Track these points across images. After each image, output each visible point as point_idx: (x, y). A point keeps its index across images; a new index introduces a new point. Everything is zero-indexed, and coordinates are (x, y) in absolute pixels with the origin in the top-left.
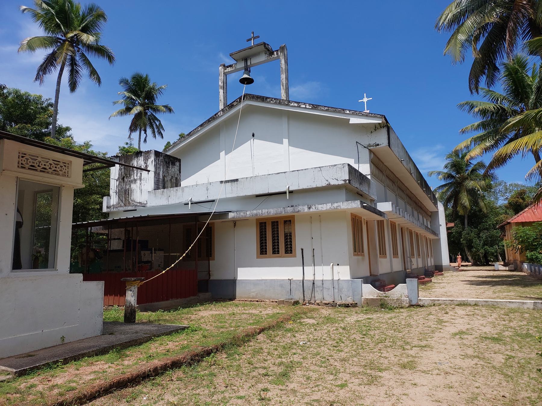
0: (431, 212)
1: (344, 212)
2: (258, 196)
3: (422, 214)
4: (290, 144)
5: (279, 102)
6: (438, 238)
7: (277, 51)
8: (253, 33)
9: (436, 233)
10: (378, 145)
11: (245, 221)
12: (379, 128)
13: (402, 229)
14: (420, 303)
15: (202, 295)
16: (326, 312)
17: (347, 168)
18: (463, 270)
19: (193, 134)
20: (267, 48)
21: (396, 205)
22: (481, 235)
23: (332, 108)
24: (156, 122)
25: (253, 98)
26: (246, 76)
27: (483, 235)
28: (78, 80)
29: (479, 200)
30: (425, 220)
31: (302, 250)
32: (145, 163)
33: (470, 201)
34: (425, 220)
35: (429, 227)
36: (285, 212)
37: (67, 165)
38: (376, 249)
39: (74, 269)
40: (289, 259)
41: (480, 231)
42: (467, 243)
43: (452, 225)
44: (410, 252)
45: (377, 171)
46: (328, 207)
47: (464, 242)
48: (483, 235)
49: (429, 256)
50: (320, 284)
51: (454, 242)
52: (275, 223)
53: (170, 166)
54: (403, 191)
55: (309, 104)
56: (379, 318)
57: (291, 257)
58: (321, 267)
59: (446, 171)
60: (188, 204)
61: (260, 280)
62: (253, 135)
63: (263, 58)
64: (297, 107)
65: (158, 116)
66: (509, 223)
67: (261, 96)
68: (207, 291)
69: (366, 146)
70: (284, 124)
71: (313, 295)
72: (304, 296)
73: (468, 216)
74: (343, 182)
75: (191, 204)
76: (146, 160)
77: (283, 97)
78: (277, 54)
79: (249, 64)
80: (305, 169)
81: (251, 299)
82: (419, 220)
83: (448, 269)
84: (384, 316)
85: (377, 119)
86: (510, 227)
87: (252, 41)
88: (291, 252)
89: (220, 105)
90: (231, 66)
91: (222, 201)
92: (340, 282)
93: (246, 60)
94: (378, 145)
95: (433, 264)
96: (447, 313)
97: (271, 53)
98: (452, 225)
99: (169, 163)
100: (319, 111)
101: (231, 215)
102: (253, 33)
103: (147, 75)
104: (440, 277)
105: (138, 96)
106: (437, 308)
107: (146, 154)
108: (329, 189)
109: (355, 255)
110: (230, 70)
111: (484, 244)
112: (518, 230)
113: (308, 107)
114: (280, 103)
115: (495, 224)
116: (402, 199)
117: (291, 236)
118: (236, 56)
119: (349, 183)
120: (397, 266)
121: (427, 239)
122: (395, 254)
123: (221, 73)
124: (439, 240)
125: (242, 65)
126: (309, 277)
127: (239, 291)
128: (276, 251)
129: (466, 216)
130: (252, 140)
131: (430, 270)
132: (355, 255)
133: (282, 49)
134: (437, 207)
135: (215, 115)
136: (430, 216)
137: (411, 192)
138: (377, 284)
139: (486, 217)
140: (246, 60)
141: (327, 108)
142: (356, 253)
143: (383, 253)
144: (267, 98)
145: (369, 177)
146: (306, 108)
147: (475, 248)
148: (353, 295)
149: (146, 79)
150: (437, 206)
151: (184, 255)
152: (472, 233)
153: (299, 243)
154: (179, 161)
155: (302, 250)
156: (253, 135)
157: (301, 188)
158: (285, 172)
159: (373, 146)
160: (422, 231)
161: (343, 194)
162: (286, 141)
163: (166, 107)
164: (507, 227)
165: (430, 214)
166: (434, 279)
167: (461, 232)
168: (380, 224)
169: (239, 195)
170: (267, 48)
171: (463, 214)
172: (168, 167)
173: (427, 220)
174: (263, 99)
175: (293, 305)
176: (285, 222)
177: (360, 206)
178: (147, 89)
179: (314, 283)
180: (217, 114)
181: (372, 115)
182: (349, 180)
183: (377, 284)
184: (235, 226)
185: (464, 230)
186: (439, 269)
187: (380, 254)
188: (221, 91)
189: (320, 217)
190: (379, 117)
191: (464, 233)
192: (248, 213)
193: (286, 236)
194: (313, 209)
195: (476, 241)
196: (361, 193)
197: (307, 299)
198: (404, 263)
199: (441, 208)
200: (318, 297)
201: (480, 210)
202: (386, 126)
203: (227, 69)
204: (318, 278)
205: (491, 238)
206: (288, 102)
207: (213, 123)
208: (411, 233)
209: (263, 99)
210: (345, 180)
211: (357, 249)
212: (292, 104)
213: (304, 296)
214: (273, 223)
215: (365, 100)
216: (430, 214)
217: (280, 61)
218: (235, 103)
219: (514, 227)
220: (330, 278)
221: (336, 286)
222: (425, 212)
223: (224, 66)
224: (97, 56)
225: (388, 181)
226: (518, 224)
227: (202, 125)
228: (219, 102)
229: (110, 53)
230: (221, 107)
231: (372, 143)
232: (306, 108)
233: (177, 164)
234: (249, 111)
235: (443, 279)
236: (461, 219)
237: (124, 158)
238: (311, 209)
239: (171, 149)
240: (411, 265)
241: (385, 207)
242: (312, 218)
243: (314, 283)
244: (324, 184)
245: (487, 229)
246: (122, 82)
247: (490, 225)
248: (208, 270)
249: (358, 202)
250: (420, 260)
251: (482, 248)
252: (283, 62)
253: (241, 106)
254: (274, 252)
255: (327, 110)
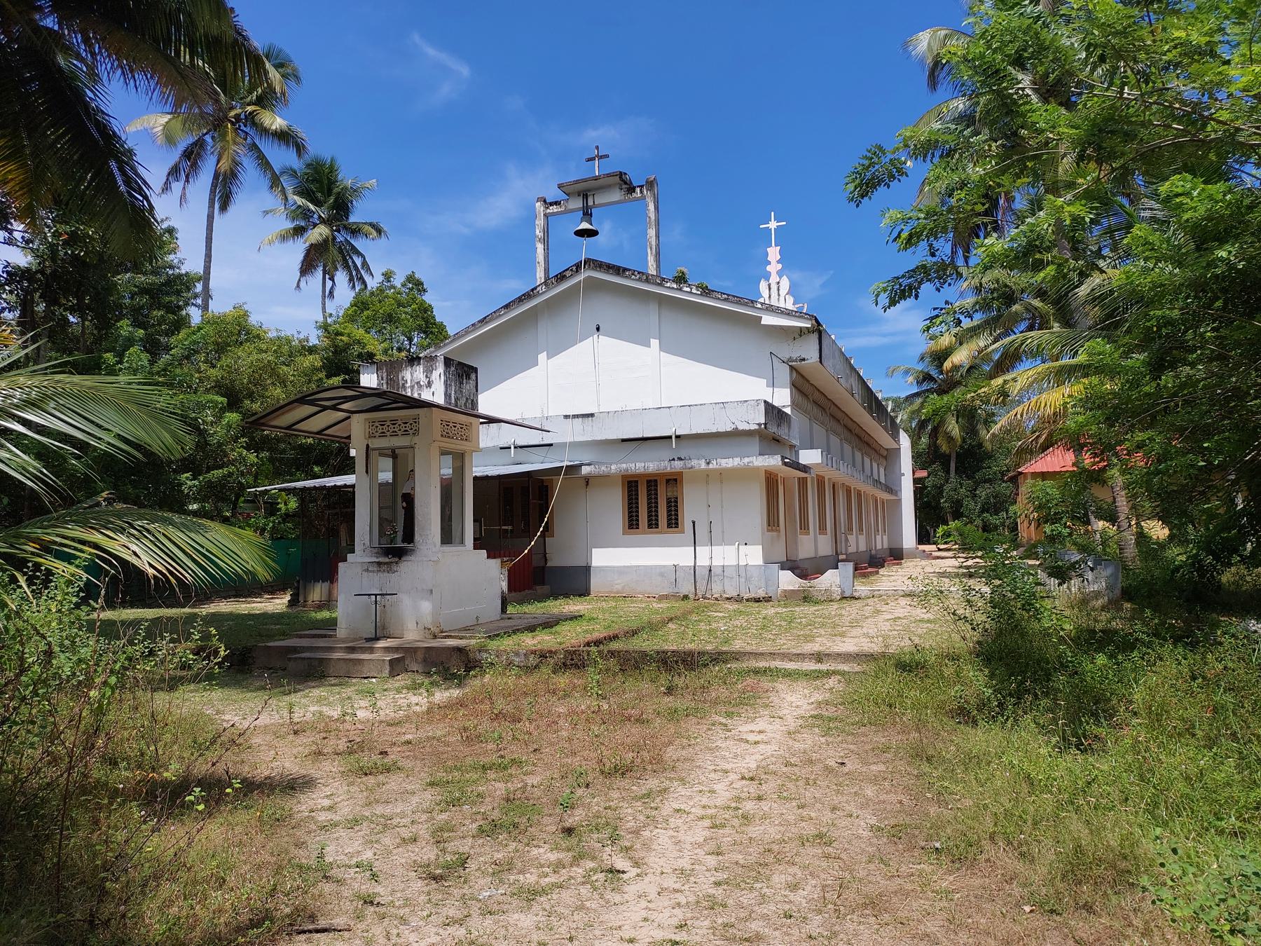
0: (887, 450)
1: (758, 468)
2: (624, 440)
3: (869, 456)
4: (662, 349)
5: (648, 279)
6: (895, 498)
7: (642, 186)
8: (597, 148)
9: (892, 489)
10: (804, 360)
11: (604, 479)
12: (806, 332)
13: (834, 485)
14: (855, 594)
15: (540, 589)
16: (732, 606)
17: (762, 406)
18: (938, 558)
19: (491, 320)
20: (623, 180)
21: (827, 451)
22: (978, 492)
23: (734, 296)
24: (355, 258)
25: (600, 267)
26: (585, 226)
27: (983, 492)
28: (234, 189)
29: (980, 426)
30: (875, 465)
31: (694, 523)
32: (427, 377)
33: (962, 428)
34: (875, 465)
35: (883, 480)
36: (671, 468)
37: (465, 427)
38: (796, 522)
39: (475, 548)
40: (672, 536)
41: (977, 484)
42: (952, 507)
43: (923, 474)
44: (845, 525)
45: (800, 398)
46: (736, 464)
47: (947, 505)
48: (983, 492)
49: (878, 531)
50: (719, 571)
51: (928, 505)
52: (652, 482)
53: (465, 380)
54: (839, 421)
55: (697, 287)
56: (802, 610)
57: (676, 532)
58: (720, 548)
59: (920, 367)
60: (510, 448)
61: (628, 567)
62: (598, 329)
63: (616, 195)
64: (677, 289)
65: (359, 243)
66: (1021, 473)
67: (614, 266)
68: (543, 583)
69: (785, 360)
70: (652, 315)
71: (709, 587)
72: (696, 589)
73: (958, 455)
74: (757, 427)
75: (515, 448)
76: (428, 372)
77: (652, 270)
78: (641, 192)
79: (590, 203)
80: (701, 405)
81: (615, 593)
82: (863, 471)
83: (913, 555)
84: (810, 609)
85: (800, 320)
86: (1026, 478)
87: (597, 162)
88: (677, 525)
89: (538, 270)
90: (557, 203)
91: (574, 445)
92: (748, 568)
93: (585, 195)
94: (804, 360)
95: (886, 546)
96: (887, 604)
97: (631, 190)
98: (923, 474)
99: (462, 375)
100: (711, 299)
101: (585, 470)
102: (597, 148)
103: (332, 160)
104: (895, 568)
105: (318, 203)
106: (876, 600)
107: (428, 362)
108: (736, 435)
109: (768, 531)
110: (555, 211)
111: (983, 510)
112: (1034, 486)
113: (694, 291)
114: (647, 281)
115: (1006, 471)
116: (837, 434)
117: (676, 502)
118: (567, 189)
119: (765, 428)
120: (825, 546)
121: (876, 501)
122: (822, 529)
123: (540, 213)
124: (898, 502)
125: (577, 203)
126: (703, 561)
127: (595, 583)
128: (653, 524)
129: (954, 456)
130: (596, 336)
131: (878, 556)
132: (768, 531)
133: (651, 184)
134: (898, 442)
135: (532, 290)
136: (886, 458)
137: (852, 420)
138: (797, 571)
139: (990, 457)
140: (585, 195)
141: (726, 296)
142: (770, 528)
143: (804, 527)
144: (625, 270)
145: (788, 410)
146: (691, 292)
147: (966, 517)
148: (767, 586)
149: (332, 169)
150: (899, 440)
151: (541, 529)
152: (961, 488)
153: (690, 510)
154: (475, 370)
155: (694, 523)
156: (598, 329)
157: (694, 432)
158: (669, 407)
159: (795, 361)
160: (868, 489)
161: (755, 445)
162: (655, 343)
163: (372, 225)
164: (1021, 479)
165: (885, 453)
166: (882, 571)
167: (942, 486)
168: (802, 482)
169: (596, 439)
170: (623, 180)
171: (948, 452)
172: (461, 383)
173: (878, 465)
174: (618, 270)
175: (682, 600)
176: (668, 481)
177: (780, 463)
178: (336, 190)
179: (710, 570)
180: (535, 288)
181: (797, 314)
182: (765, 424)
183: (797, 571)
184: (587, 485)
185: (947, 482)
186: (897, 555)
187: (820, 529)
188: (540, 247)
189: (722, 475)
190: (807, 319)
191: (947, 488)
192: (613, 467)
193: (669, 501)
194: (713, 465)
195: (969, 504)
196: (778, 438)
197: (700, 594)
198: (836, 542)
199: (905, 441)
200: (716, 589)
201: (980, 445)
202: (818, 330)
203: (551, 208)
204: (717, 562)
205: (995, 498)
206: (661, 282)
207: (526, 305)
208: (848, 491)
209: (619, 270)
210: (759, 425)
211: (772, 521)
212: (668, 285)
213: (696, 589)
214: (649, 482)
215: (773, 225)
216: (886, 452)
217: (647, 205)
218: (568, 274)
219: (1029, 481)
220: (735, 563)
221: (743, 574)
222: (875, 451)
223: (545, 201)
224: (276, 146)
225: (816, 410)
226: (1035, 475)
227: (507, 306)
228: (536, 266)
229: (299, 140)
230: (540, 276)
231: (795, 356)
232: (691, 292)
233: (473, 376)
234: (593, 286)
235: (899, 570)
236: (944, 460)
237: (387, 366)
238: (711, 465)
239: (451, 342)
240: (846, 547)
241: (810, 457)
242: (709, 477)
243: (710, 570)
244: (729, 428)
245: (989, 481)
246: (284, 172)
247: (995, 473)
248: (543, 552)
249: (778, 458)
250: (862, 539)
251: (979, 516)
252: (651, 207)
253: (582, 276)
254: (650, 526)
255: (725, 300)
